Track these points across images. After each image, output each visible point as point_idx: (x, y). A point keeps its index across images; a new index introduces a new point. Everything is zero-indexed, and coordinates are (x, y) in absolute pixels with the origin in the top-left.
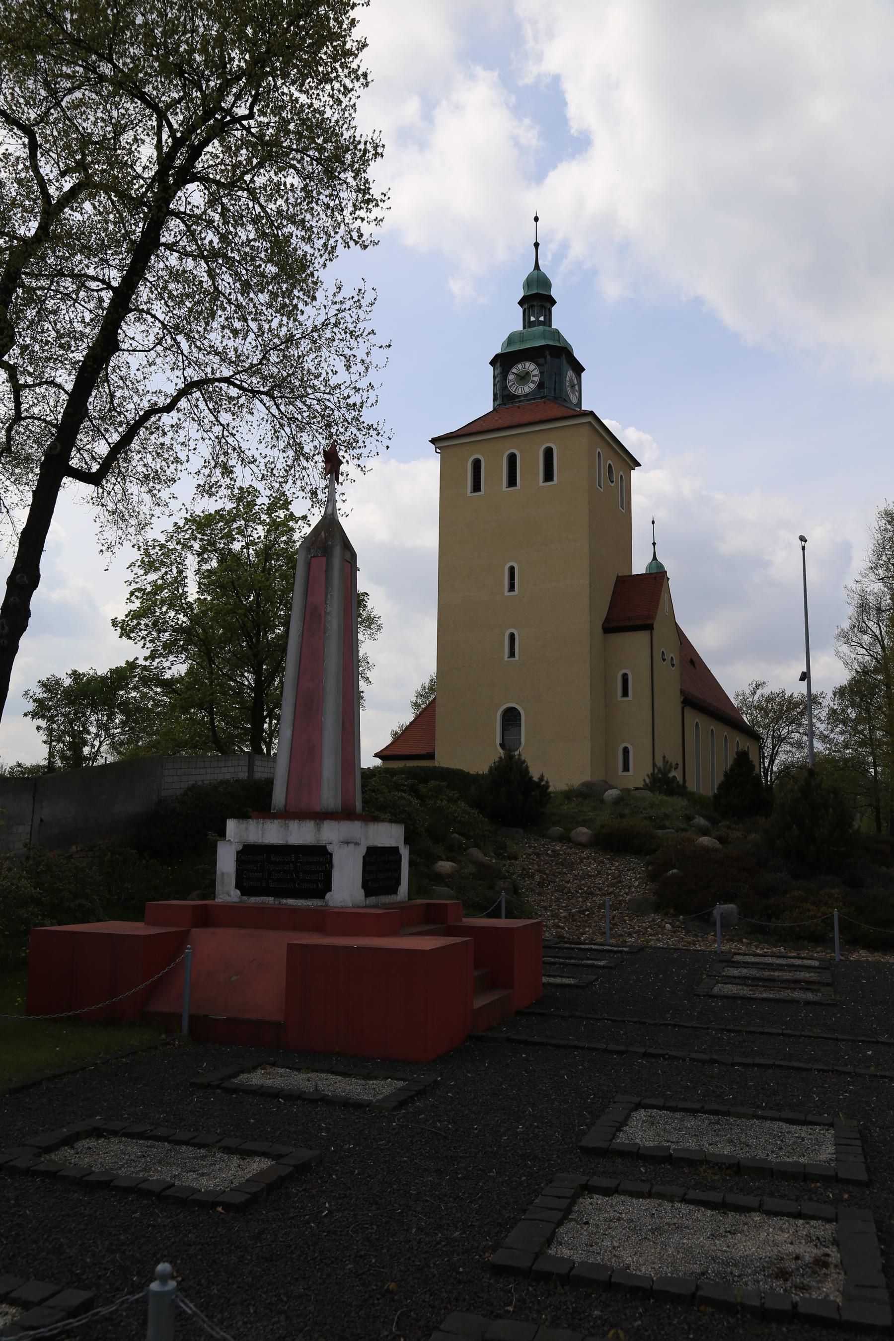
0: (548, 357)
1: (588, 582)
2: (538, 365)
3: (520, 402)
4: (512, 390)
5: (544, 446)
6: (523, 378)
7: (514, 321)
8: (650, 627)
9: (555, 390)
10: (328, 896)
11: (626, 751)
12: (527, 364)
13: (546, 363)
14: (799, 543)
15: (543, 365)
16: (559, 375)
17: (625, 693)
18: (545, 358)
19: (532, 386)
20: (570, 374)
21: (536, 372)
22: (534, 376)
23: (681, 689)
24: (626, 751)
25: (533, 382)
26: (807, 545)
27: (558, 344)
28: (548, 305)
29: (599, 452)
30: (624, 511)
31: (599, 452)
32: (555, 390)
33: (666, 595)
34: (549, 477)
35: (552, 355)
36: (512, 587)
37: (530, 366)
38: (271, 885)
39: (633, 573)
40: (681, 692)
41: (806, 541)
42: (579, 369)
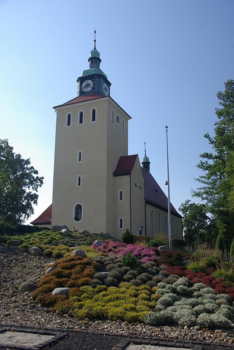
0: (96, 78)
1: (106, 157)
3: (86, 94)
4: (84, 90)
5: (93, 108)
6: (88, 85)
7: (87, 66)
8: (130, 174)
9: (98, 90)
11: (121, 220)
12: (89, 81)
14: (165, 129)
15: (94, 81)
16: (100, 84)
18: (95, 78)
19: (90, 88)
20: (105, 85)
21: (92, 83)
22: (91, 85)
23: (145, 198)
24: (121, 220)
25: (91, 87)
26: (168, 129)
27: (100, 74)
28: (98, 61)
29: (113, 111)
30: (124, 134)
31: (113, 111)
32: (98, 90)
33: (138, 163)
34: (94, 119)
36: (80, 160)
37: (90, 82)
39: (128, 155)
40: (145, 199)
41: (167, 128)
42: (109, 84)
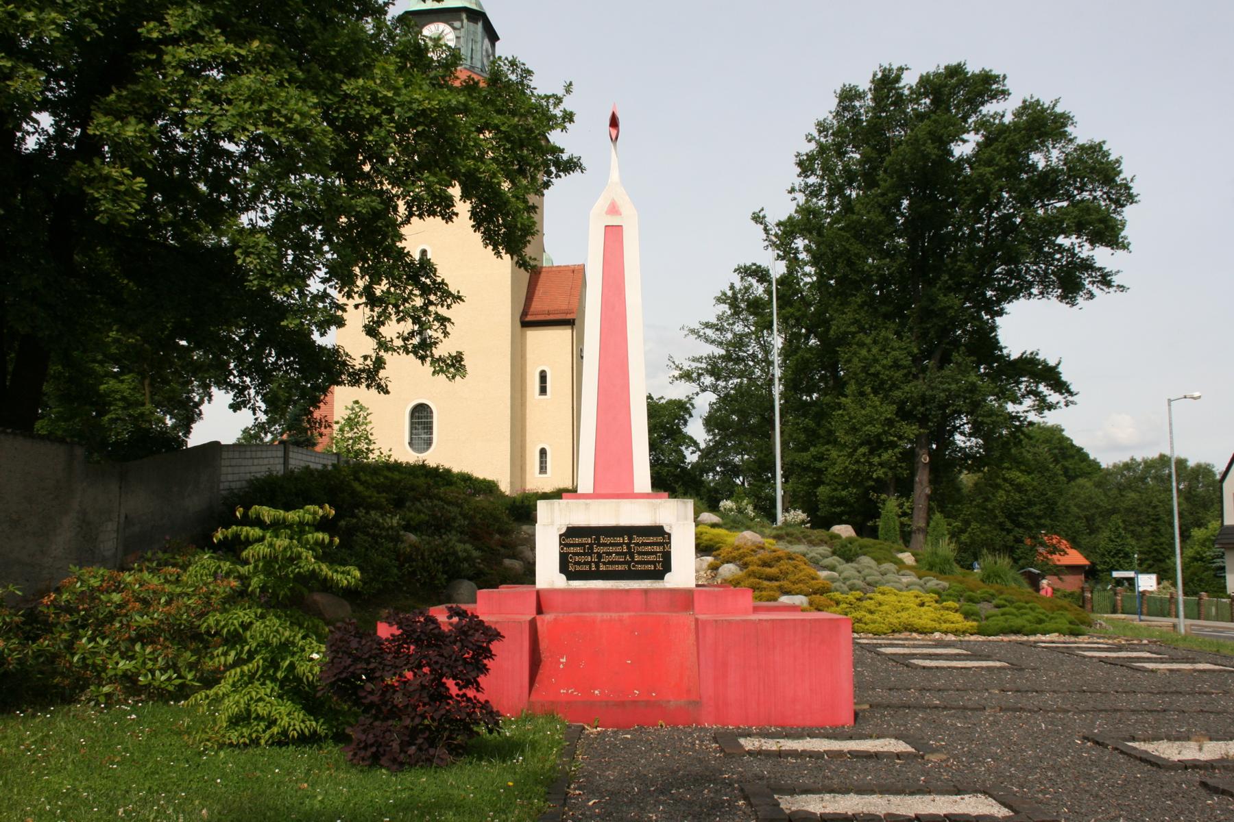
0: (465, 21)
2: (454, 28)
9: (472, 58)
10: (667, 576)
13: (462, 27)
15: (459, 29)
17: (543, 390)
32: (472, 58)
35: (469, 19)
38: (602, 568)
